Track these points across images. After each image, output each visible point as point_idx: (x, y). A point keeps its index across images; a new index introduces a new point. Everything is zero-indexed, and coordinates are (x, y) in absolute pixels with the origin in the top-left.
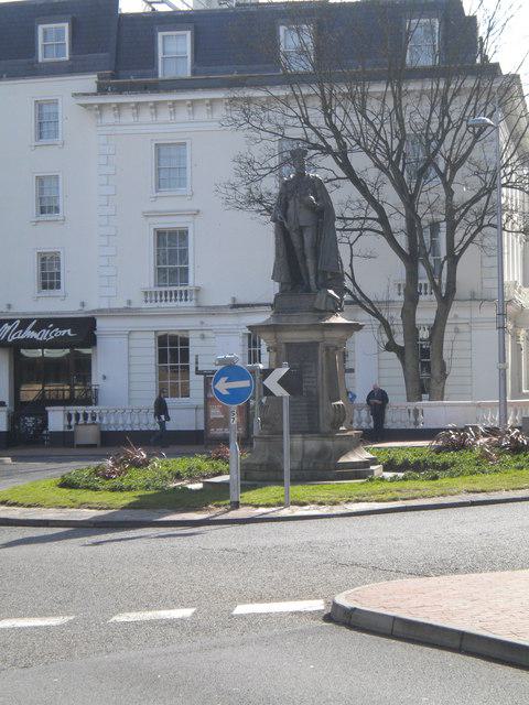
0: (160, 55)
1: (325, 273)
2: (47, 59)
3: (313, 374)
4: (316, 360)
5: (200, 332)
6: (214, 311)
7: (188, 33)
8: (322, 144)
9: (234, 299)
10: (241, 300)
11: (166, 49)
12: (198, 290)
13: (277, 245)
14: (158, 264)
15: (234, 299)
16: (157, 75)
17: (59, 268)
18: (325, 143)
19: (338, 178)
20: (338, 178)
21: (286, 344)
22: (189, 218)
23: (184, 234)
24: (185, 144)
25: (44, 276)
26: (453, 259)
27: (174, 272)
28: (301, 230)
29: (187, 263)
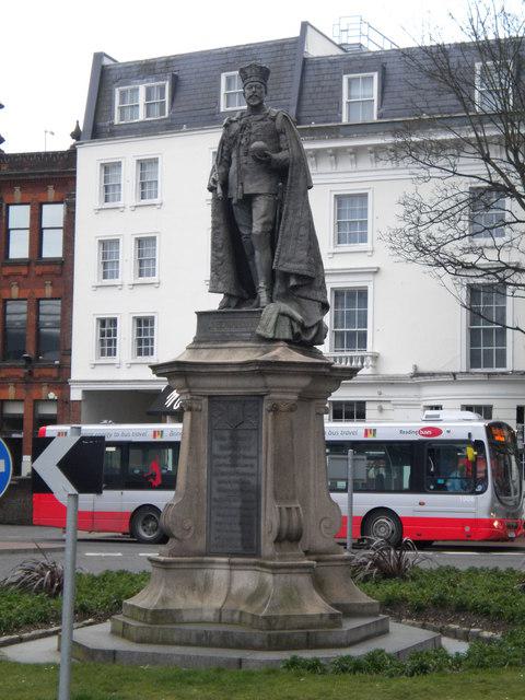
0: (345, 99)
1: (286, 276)
2: (230, 109)
3: (253, 452)
4: (258, 429)
5: (378, 404)
6: (393, 382)
7: (376, 75)
8: (502, 182)
9: (416, 367)
10: (423, 368)
11: (352, 94)
12: (375, 358)
13: (215, 228)
14: (335, 327)
15: (416, 367)
16: (341, 121)
17: (152, 335)
18: (507, 180)
19: (518, 221)
20: (518, 221)
21: (210, 397)
22: (371, 277)
23: (361, 294)
24: (366, 195)
25: (140, 342)
26: (445, 211)
27: (351, 335)
28: (248, 200)
29: (366, 327)
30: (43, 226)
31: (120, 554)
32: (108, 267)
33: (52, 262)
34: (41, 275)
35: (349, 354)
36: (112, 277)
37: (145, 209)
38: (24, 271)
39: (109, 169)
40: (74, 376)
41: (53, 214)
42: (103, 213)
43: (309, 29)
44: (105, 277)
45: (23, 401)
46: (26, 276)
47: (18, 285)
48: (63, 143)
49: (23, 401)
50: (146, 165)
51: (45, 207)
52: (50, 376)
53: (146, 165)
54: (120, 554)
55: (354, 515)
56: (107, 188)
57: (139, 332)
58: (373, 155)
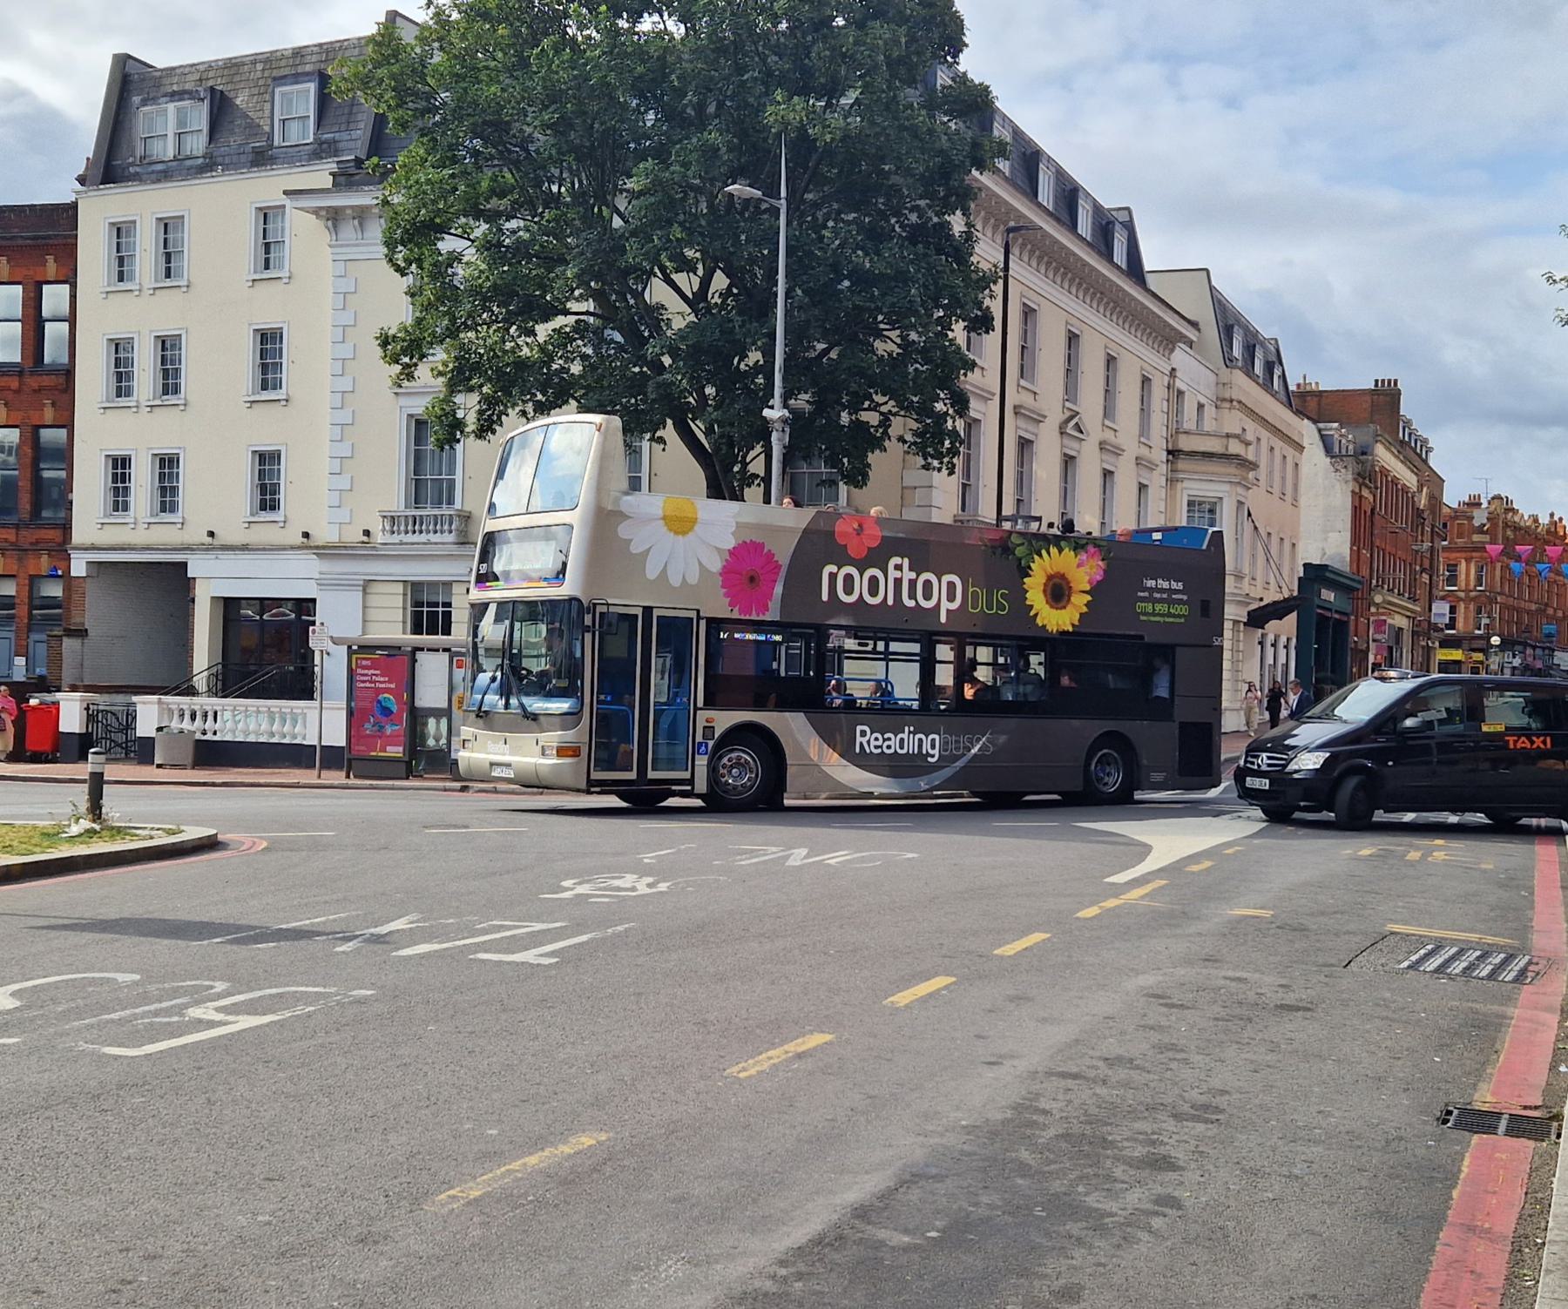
30: (45, 313)
31: (750, 1068)
32: (122, 382)
33: (55, 370)
34: (38, 391)
35: (436, 512)
36: (275, 388)
37: (164, 290)
38: (14, 384)
39: (121, 231)
40: (78, 537)
41: (54, 298)
42: (259, 286)
43: (399, 20)
44: (264, 387)
45: (14, 576)
46: (18, 391)
47: (53, 404)
48: (60, 190)
49: (14, 576)
50: (168, 226)
51: (45, 287)
52: (51, 541)
53: (168, 226)
54: (750, 1068)
55: (323, 744)
56: (267, 246)
57: (162, 476)
58: (356, 222)
